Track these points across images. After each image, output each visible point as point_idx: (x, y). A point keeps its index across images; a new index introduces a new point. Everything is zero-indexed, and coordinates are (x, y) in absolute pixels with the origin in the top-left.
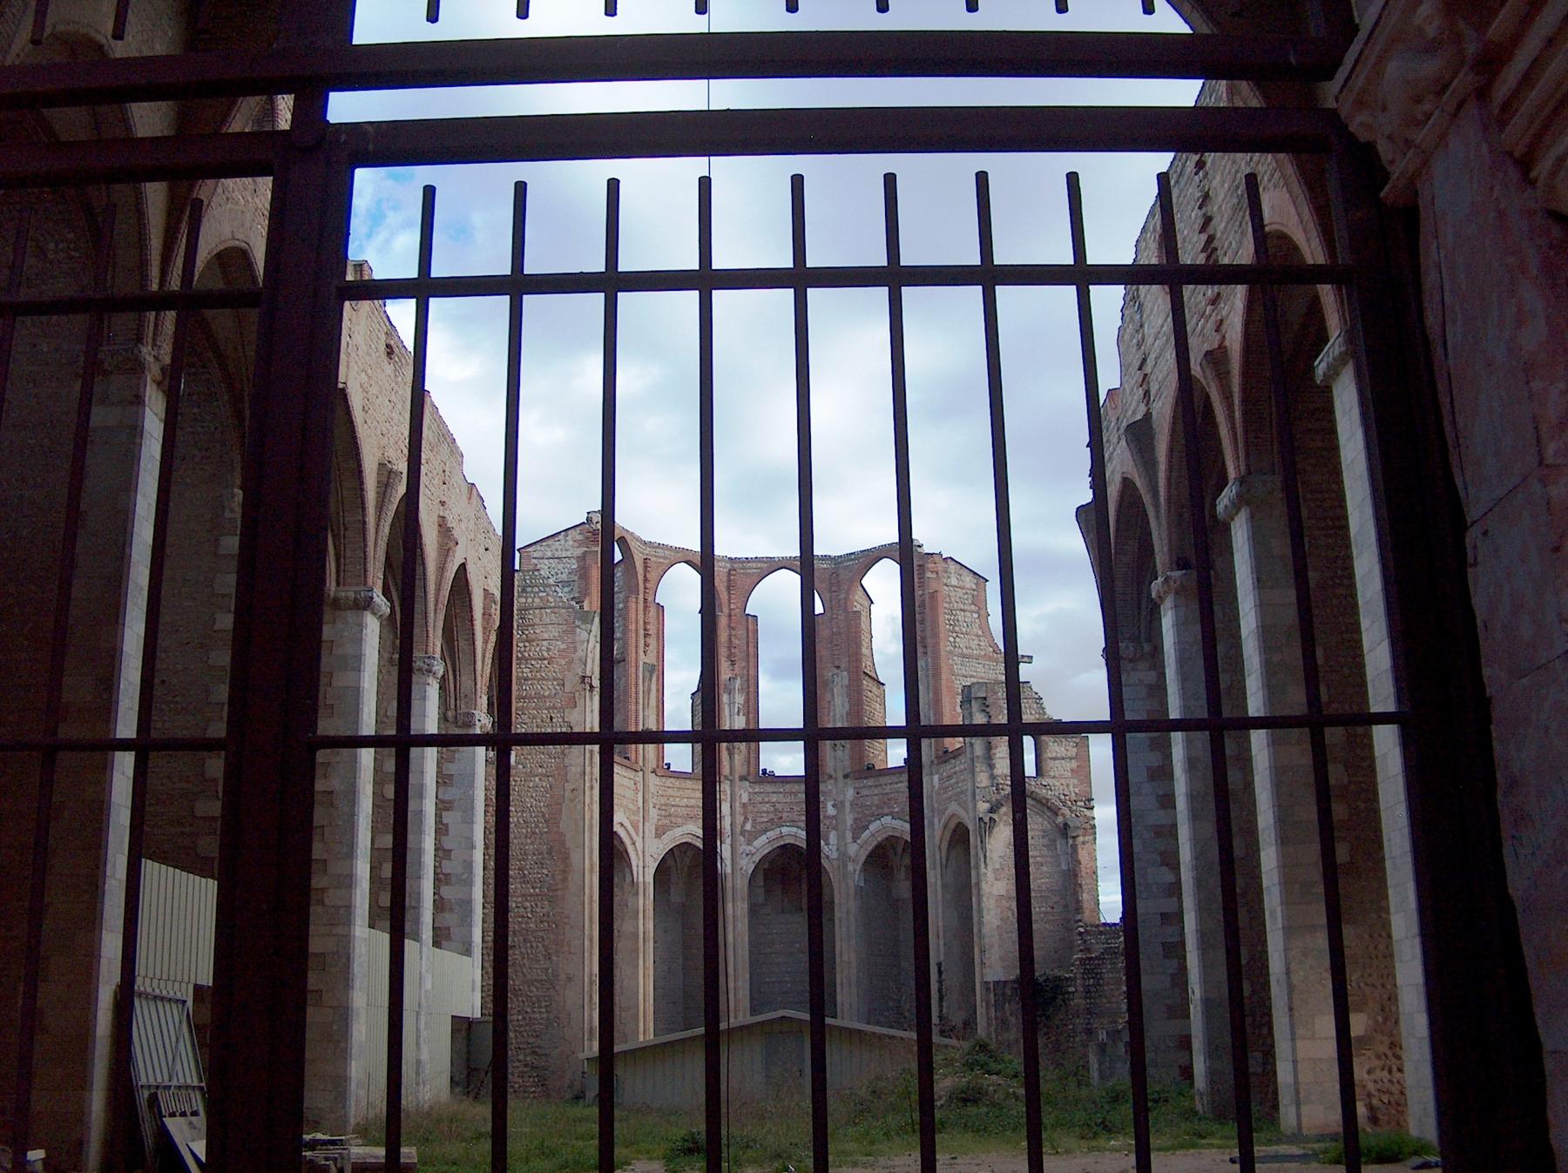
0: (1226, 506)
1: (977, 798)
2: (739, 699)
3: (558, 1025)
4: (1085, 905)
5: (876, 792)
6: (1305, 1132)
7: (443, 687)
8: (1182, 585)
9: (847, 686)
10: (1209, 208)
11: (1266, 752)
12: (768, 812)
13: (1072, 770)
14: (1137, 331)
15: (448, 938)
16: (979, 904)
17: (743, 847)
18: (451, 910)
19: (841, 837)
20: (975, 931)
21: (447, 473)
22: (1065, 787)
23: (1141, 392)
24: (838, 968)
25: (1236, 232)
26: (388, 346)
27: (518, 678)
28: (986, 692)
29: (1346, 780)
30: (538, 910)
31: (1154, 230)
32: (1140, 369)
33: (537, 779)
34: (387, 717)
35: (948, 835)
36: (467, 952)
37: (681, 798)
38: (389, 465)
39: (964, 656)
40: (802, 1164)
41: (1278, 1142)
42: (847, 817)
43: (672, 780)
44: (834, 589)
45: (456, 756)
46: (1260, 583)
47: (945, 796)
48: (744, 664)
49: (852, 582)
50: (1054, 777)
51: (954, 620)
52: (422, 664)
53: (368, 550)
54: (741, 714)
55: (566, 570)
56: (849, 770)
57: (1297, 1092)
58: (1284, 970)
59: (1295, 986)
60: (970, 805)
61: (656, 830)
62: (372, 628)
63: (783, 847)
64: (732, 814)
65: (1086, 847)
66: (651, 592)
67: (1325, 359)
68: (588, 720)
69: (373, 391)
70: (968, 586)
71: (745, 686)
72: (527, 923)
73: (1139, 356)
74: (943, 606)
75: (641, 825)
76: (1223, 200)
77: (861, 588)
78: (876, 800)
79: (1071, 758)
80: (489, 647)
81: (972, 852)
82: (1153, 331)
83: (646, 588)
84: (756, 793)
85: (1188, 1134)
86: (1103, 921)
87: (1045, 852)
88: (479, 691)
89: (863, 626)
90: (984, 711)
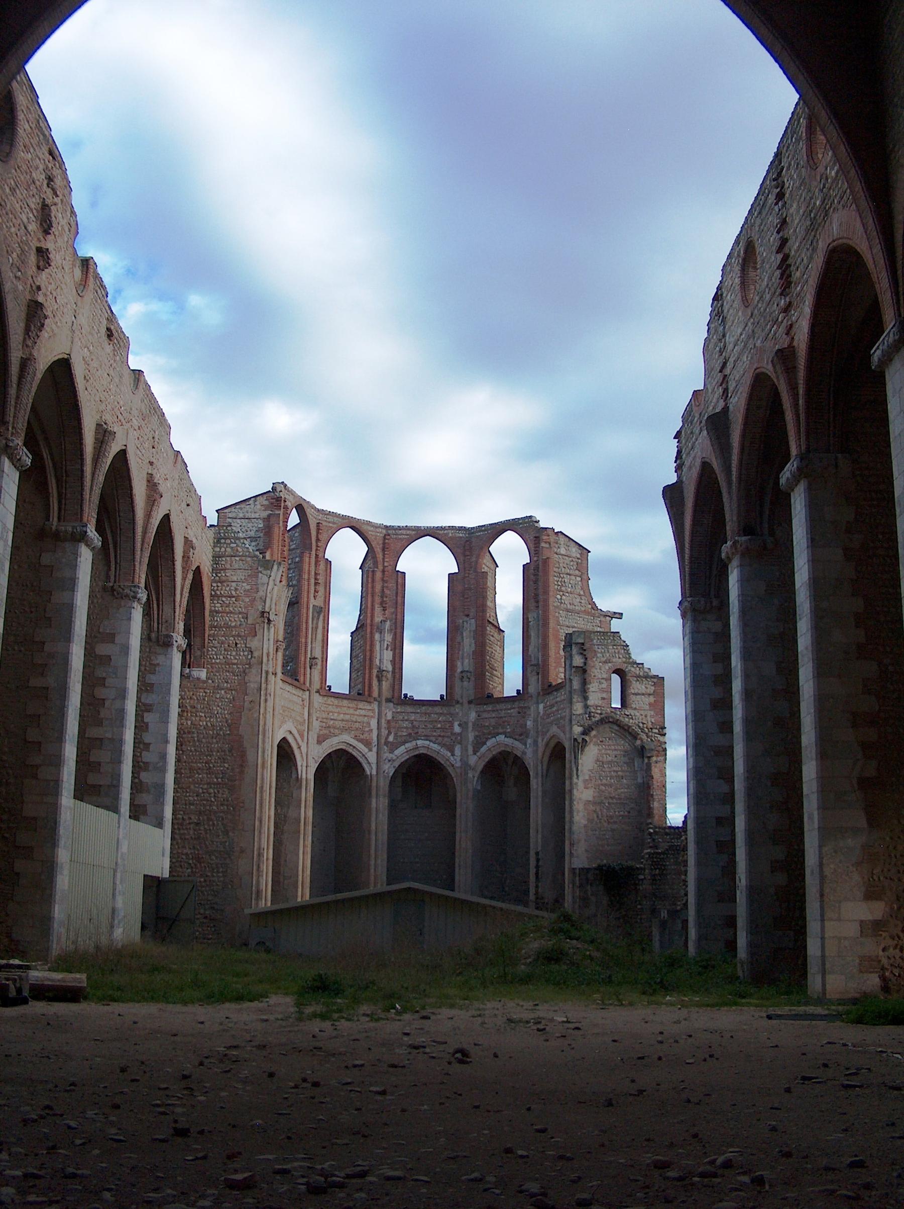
0: (788, 479)
1: (573, 723)
2: (388, 638)
3: (232, 887)
4: (655, 812)
5: (494, 715)
6: (828, 997)
7: (147, 613)
8: (747, 548)
9: (474, 631)
10: (786, 231)
11: (811, 683)
12: (406, 728)
13: (650, 704)
14: (720, 340)
15: (145, 813)
16: (571, 807)
17: (387, 755)
18: (148, 791)
19: (464, 750)
20: (567, 827)
21: (156, 439)
22: (643, 717)
23: (721, 390)
24: (457, 854)
25: (808, 249)
26: (108, 329)
27: (211, 611)
28: (584, 638)
29: (877, 708)
30: (220, 795)
31: (738, 256)
32: (721, 371)
33: (223, 692)
34: (99, 632)
35: (548, 753)
36: (160, 825)
37: (339, 713)
38: (105, 426)
39: (568, 610)
40: (409, 1004)
41: (806, 1004)
42: (470, 735)
43: (333, 699)
44: (468, 553)
45: (157, 669)
46: (813, 542)
47: (548, 720)
48: (393, 610)
49: (482, 548)
50: (635, 709)
51: (561, 582)
52: (129, 592)
53: (84, 493)
54: (389, 648)
55: (254, 529)
56: (473, 698)
57: (824, 964)
58: (818, 863)
59: (826, 876)
60: (567, 728)
61: (318, 737)
62: (86, 558)
63: (419, 756)
64: (379, 728)
65: (658, 765)
66: (322, 550)
67: (881, 347)
68: (265, 646)
69: (95, 364)
70: (574, 555)
71: (393, 628)
72: (210, 806)
73: (721, 360)
74: (553, 570)
75: (306, 734)
76: (798, 224)
77: (488, 554)
78: (493, 722)
79: (650, 695)
80: (186, 583)
81: (567, 766)
82: (732, 339)
83: (317, 546)
84: (398, 712)
85: (730, 994)
86: (669, 825)
87: (625, 768)
88: (177, 618)
89: (489, 584)
90: (582, 654)
